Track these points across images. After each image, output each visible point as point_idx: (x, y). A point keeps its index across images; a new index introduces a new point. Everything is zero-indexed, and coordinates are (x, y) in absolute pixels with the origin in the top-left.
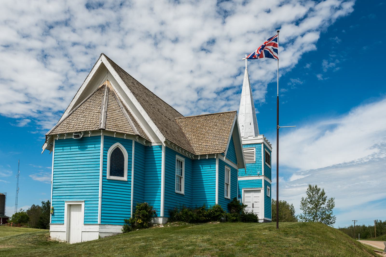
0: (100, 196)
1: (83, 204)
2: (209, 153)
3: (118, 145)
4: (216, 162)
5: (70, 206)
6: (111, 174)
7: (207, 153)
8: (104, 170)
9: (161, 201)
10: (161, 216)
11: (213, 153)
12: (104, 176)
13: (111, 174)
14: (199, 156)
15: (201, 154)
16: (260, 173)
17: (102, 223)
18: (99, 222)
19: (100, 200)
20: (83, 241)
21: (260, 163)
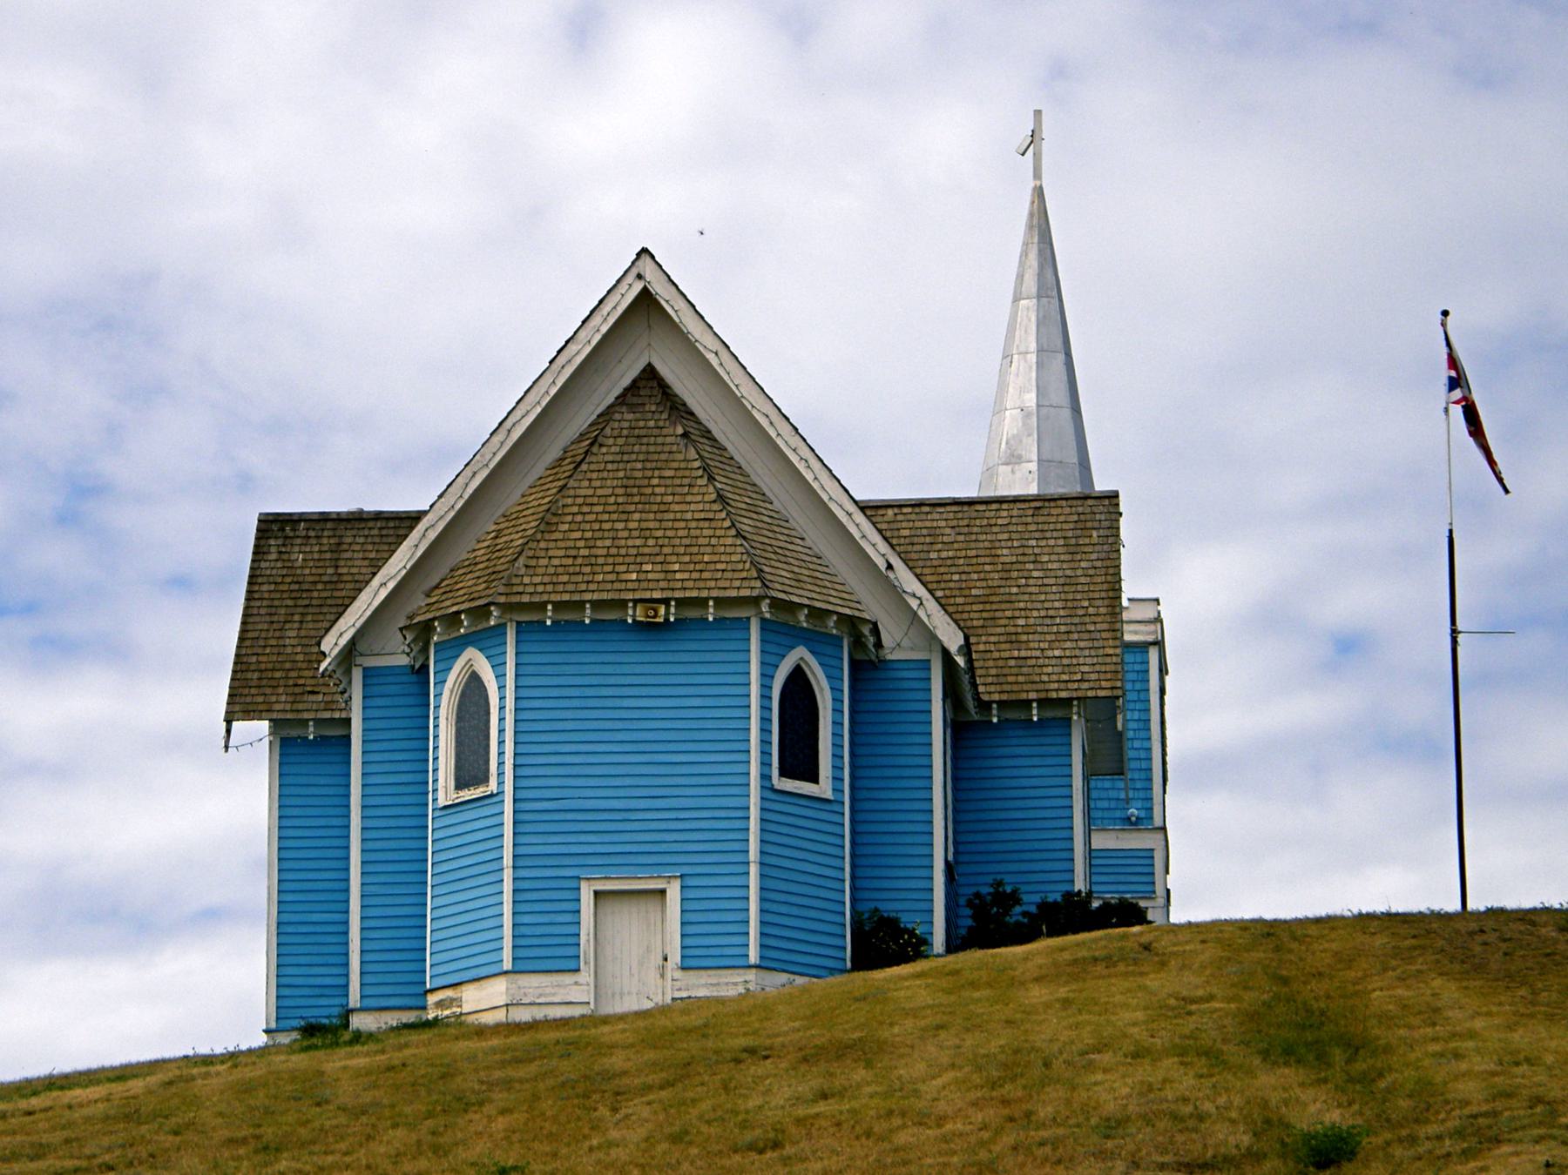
0: (754, 854)
1: (674, 892)
2: (1043, 695)
3: (802, 659)
4: (1070, 735)
5: (596, 893)
6: (783, 773)
7: (1032, 696)
8: (765, 764)
9: (1157, 883)
10: (505, 969)
11: (1063, 695)
12: (765, 777)
13: (783, 773)
14: (995, 706)
15: (1004, 697)
16: (1143, 814)
17: (764, 964)
18: (753, 957)
19: (754, 870)
20: (510, 1020)
21: (1143, 754)
